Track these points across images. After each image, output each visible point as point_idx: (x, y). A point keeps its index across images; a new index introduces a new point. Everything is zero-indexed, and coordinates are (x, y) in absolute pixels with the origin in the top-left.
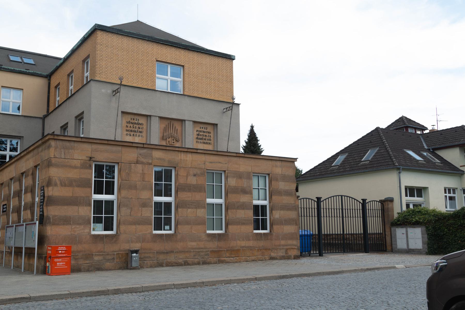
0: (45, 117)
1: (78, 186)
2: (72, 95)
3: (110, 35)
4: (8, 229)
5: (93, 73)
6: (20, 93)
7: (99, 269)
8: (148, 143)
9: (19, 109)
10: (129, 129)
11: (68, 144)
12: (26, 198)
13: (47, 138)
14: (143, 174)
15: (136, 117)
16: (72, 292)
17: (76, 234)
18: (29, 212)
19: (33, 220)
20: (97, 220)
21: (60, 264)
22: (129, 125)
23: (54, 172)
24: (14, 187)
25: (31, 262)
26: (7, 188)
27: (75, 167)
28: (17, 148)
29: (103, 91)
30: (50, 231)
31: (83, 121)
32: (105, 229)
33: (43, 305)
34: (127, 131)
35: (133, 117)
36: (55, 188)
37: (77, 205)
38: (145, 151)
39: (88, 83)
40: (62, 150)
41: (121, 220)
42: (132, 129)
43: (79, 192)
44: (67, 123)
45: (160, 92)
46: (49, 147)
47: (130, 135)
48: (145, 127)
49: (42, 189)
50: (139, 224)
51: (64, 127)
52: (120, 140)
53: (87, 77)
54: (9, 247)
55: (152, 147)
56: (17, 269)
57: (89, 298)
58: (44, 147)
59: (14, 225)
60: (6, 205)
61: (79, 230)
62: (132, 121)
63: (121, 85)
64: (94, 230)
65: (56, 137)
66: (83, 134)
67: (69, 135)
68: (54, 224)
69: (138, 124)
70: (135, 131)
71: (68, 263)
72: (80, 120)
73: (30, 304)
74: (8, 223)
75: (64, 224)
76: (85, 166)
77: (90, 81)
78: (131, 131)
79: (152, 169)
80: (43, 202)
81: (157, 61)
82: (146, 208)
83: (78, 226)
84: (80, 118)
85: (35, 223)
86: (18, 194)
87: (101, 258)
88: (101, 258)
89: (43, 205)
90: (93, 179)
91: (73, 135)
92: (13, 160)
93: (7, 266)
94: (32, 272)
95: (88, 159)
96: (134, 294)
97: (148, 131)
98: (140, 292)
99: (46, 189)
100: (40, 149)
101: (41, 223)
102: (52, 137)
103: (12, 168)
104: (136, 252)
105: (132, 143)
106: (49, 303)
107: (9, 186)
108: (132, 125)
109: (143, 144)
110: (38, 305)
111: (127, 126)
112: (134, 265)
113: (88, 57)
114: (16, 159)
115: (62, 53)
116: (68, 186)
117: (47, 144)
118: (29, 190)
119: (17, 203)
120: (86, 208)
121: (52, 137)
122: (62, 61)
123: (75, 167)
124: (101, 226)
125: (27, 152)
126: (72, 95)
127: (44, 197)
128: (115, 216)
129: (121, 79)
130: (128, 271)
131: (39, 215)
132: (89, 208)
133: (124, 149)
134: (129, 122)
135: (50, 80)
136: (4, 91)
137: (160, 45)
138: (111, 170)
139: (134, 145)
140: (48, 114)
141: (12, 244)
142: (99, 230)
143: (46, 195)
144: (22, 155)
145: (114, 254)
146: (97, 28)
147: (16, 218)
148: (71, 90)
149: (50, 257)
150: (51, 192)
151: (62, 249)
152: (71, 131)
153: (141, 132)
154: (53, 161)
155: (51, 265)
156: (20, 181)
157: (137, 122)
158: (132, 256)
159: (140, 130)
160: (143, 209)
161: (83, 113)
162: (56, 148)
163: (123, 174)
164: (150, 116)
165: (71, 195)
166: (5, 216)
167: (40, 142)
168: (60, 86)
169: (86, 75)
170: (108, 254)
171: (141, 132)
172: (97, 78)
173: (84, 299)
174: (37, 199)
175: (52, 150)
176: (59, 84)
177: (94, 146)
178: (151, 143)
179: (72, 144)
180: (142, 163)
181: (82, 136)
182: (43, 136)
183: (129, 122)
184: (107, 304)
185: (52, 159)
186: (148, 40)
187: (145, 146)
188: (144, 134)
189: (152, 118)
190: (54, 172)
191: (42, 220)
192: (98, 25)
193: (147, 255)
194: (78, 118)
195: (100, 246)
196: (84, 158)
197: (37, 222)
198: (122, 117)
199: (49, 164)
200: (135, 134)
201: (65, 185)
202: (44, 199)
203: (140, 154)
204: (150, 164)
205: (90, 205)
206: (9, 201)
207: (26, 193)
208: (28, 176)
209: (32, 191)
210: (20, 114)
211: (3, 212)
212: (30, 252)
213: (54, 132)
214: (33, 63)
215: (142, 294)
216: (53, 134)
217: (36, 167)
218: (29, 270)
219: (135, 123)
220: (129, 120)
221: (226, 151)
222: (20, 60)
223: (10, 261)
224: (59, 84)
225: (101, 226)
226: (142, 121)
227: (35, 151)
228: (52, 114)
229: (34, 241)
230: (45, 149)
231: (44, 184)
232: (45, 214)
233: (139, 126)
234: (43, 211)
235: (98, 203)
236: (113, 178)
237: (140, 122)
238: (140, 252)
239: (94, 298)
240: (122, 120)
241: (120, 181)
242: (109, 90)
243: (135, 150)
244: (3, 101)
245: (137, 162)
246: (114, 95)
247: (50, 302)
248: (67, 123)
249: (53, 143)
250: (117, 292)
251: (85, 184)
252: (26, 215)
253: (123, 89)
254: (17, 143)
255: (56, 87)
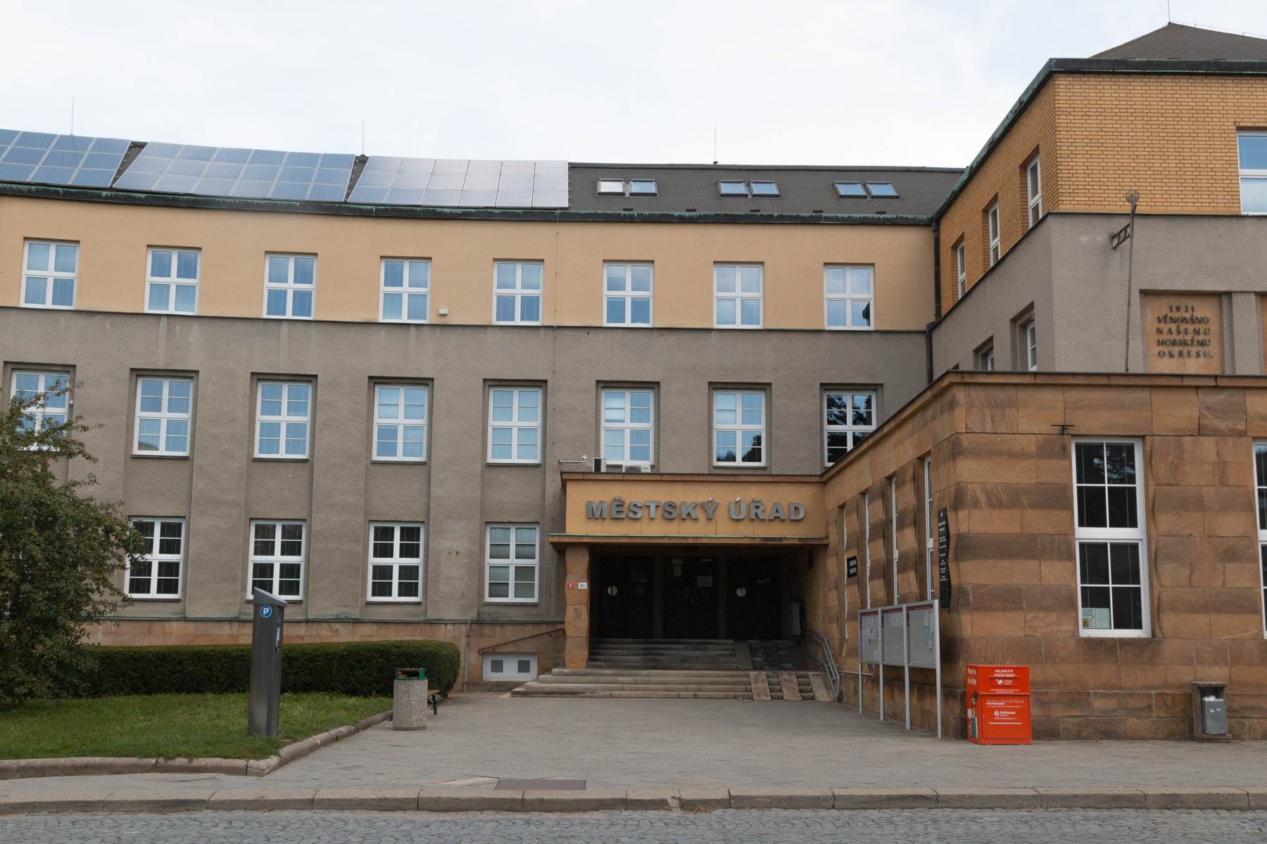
0: (933, 327)
1: (1035, 506)
2: (999, 263)
3: (1093, 81)
4: (866, 620)
5: (1052, 193)
6: (867, 273)
7: (1107, 732)
8: (1228, 372)
9: (866, 314)
10: (1164, 337)
11: (999, 394)
12: (902, 541)
13: (945, 382)
14: (1222, 465)
15: (1185, 302)
16: (1042, 791)
17: (1038, 634)
18: (912, 576)
19: (923, 596)
20: (1094, 599)
21: (1002, 714)
22: (1165, 328)
23: (969, 471)
24: (872, 513)
25: (927, 706)
26: (855, 515)
27: (1025, 456)
28: (869, 414)
29: (1083, 239)
30: (971, 625)
31: (1033, 330)
32: (1119, 625)
33: (973, 819)
34: (1160, 343)
35: (1174, 302)
36: (976, 514)
37: (1034, 557)
38: (1221, 397)
39: (1039, 223)
40: (987, 412)
41: (1163, 598)
42: (1174, 336)
43: (1039, 522)
44: (991, 339)
45: (1253, 221)
46: (953, 405)
47: (1171, 355)
48: (1214, 327)
49: (942, 516)
50: (1218, 611)
51: (984, 351)
52: (1141, 371)
53: (1036, 209)
54: (869, 665)
55: (1244, 383)
56: (894, 720)
57: (1092, 813)
58: (937, 406)
59: (879, 610)
60: (854, 558)
61: (1045, 625)
62: (1175, 315)
63: (1133, 215)
64: (1086, 625)
65: (967, 379)
66: (1034, 363)
67: (997, 369)
68: (978, 608)
69: (1193, 321)
70: (1185, 343)
71: (1022, 714)
72: (1024, 327)
73: (939, 813)
74: (864, 605)
75: (1004, 609)
76: (1051, 449)
77: (1045, 218)
78: (1174, 343)
79: (1249, 450)
80: (946, 551)
81: (1240, 129)
82: (1239, 565)
83: (1042, 615)
84: (1023, 321)
85: (931, 606)
86: (882, 531)
87: (1111, 704)
88: (1111, 704)
89: (946, 558)
90: (1075, 485)
91: (1009, 369)
92: (865, 446)
93: (870, 712)
94: (932, 732)
95: (1057, 430)
96: (1224, 813)
97: (1226, 338)
98: (1242, 809)
99: (951, 515)
100: (930, 413)
101: (945, 605)
102: (956, 379)
103: (864, 463)
104: (1217, 691)
105: (1181, 376)
106: (987, 815)
107: (859, 511)
108: (1173, 327)
109: (1216, 377)
110: (961, 819)
111: (1160, 331)
112: (1212, 727)
113: (1036, 152)
114: (871, 442)
115: (962, 156)
116: (1011, 507)
117: (947, 398)
118: (909, 520)
119: (881, 554)
120: (1059, 565)
121: (956, 379)
122: (964, 177)
123: (1025, 456)
124: (1106, 614)
125: (895, 422)
126: (999, 263)
127: (948, 536)
128: (1144, 585)
129: (1133, 199)
130: (1196, 745)
131: (937, 585)
132: (1069, 564)
133: (1159, 397)
134: (1164, 319)
135: (937, 231)
136: (829, 277)
137: (1244, 81)
138: (1122, 457)
139: (1187, 382)
140: (940, 319)
141: (876, 656)
142: (1100, 626)
143: (952, 532)
144: (886, 430)
145: (1149, 696)
146: (1058, 70)
147: (881, 594)
148: (996, 249)
149: (976, 695)
150: (966, 523)
151: (1003, 675)
152: (1002, 358)
153: (1202, 344)
154: (965, 441)
155: (979, 714)
156: (885, 497)
157: (1188, 315)
158: (1203, 703)
159: (1201, 338)
160: (1228, 565)
161: (1031, 307)
162: (970, 406)
163: (1161, 469)
164: (1229, 294)
165: (1017, 530)
166: (856, 587)
167: (928, 395)
168: (964, 244)
169: (1032, 202)
170: (1131, 695)
171: (1202, 344)
172: (1063, 208)
173: (1078, 814)
174: (930, 543)
175: (960, 413)
176: (961, 238)
177: (1072, 395)
178: (1239, 373)
179: (1011, 392)
180: (1217, 433)
181: (1033, 369)
182: (932, 382)
183: (1164, 319)
184: (1148, 833)
185: (963, 437)
186: (1206, 75)
187: (1221, 382)
188: (1213, 349)
189: (1235, 298)
190: (969, 471)
191: (947, 595)
192: (1058, 60)
193: (1249, 702)
194: (1020, 322)
195: (1106, 672)
196: (1045, 428)
197: (936, 603)
198: (1142, 305)
199: (955, 450)
200: (1185, 350)
201: (1001, 505)
202: (948, 543)
203: (1208, 408)
204: (1241, 434)
205: (1071, 557)
206: (861, 548)
207: (901, 527)
208: (904, 483)
209: (918, 524)
210: (871, 328)
211: (850, 575)
212: (922, 679)
213: (957, 367)
214: (893, 193)
215: (1250, 815)
216: (956, 370)
217: (921, 459)
218: (924, 726)
219: (1184, 320)
220: (1165, 311)
221: (1123, 371)
222: (862, 192)
223: (874, 701)
224: (961, 238)
225: (1106, 614)
226: (1204, 310)
227: (917, 418)
228: (948, 319)
229: (932, 650)
230: (942, 412)
231: (947, 503)
232: (954, 582)
233: (1197, 326)
234: (947, 574)
235: (1093, 552)
236: (1132, 479)
237: (1198, 314)
238: (1226, 691)
239: (1106, 813)
240: (1143, 314)
241: (1152, 488)
242: (1099, 234)
243: (1191, 396)
244: (829, 300)
245: (1201, 431)
246: (1115, 248)
247: (988, 813)
248: (991, 339)
249: (960, 394)
250: (1171, 802)
251: (1053, 498)
252: (904, 583)
253: (1140, 228)
254: (868, 402)
255: (955, 247)
